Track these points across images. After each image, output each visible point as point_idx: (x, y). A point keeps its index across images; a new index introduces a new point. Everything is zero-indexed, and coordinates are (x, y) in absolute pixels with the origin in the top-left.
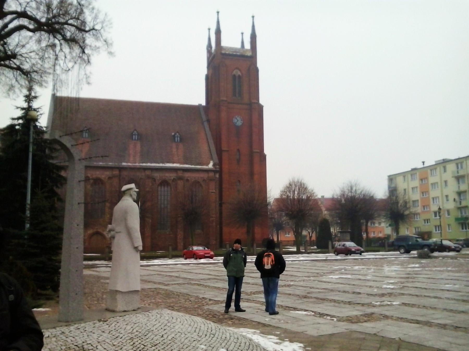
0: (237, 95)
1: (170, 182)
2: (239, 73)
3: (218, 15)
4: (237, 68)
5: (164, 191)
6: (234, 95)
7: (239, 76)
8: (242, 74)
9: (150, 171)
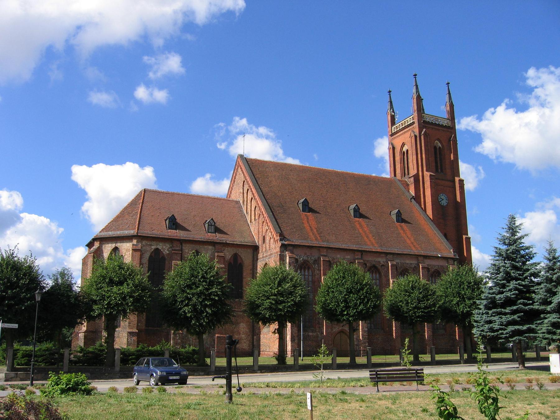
0: (439, 170)
1: (379, 267)
5: (308, 275)
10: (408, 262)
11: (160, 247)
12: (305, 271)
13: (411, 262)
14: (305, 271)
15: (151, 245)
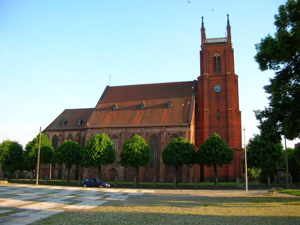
2: (219, 55)
3: (228, 17)
4: (217, 52)
6: (215, 70)
7: (218, 57)
8: (220, 56)
9: (164, 128)
10: (155, 131)
11: (56, 134)
12: (115, 139)
13: (158, 131)
14: (115, 139)
15: (53, 133)
